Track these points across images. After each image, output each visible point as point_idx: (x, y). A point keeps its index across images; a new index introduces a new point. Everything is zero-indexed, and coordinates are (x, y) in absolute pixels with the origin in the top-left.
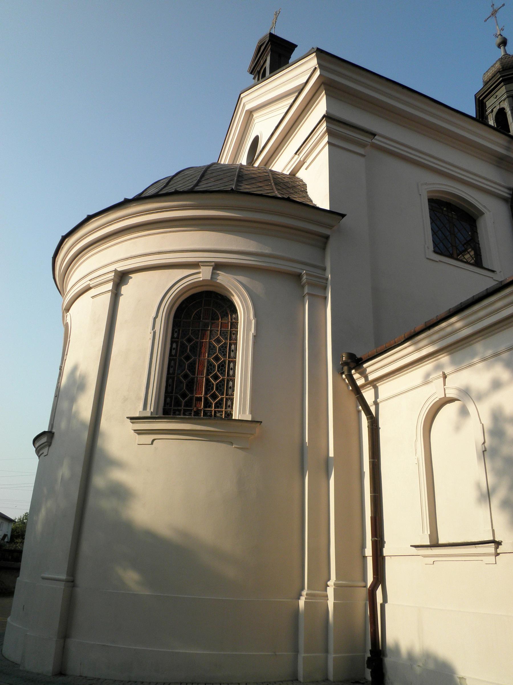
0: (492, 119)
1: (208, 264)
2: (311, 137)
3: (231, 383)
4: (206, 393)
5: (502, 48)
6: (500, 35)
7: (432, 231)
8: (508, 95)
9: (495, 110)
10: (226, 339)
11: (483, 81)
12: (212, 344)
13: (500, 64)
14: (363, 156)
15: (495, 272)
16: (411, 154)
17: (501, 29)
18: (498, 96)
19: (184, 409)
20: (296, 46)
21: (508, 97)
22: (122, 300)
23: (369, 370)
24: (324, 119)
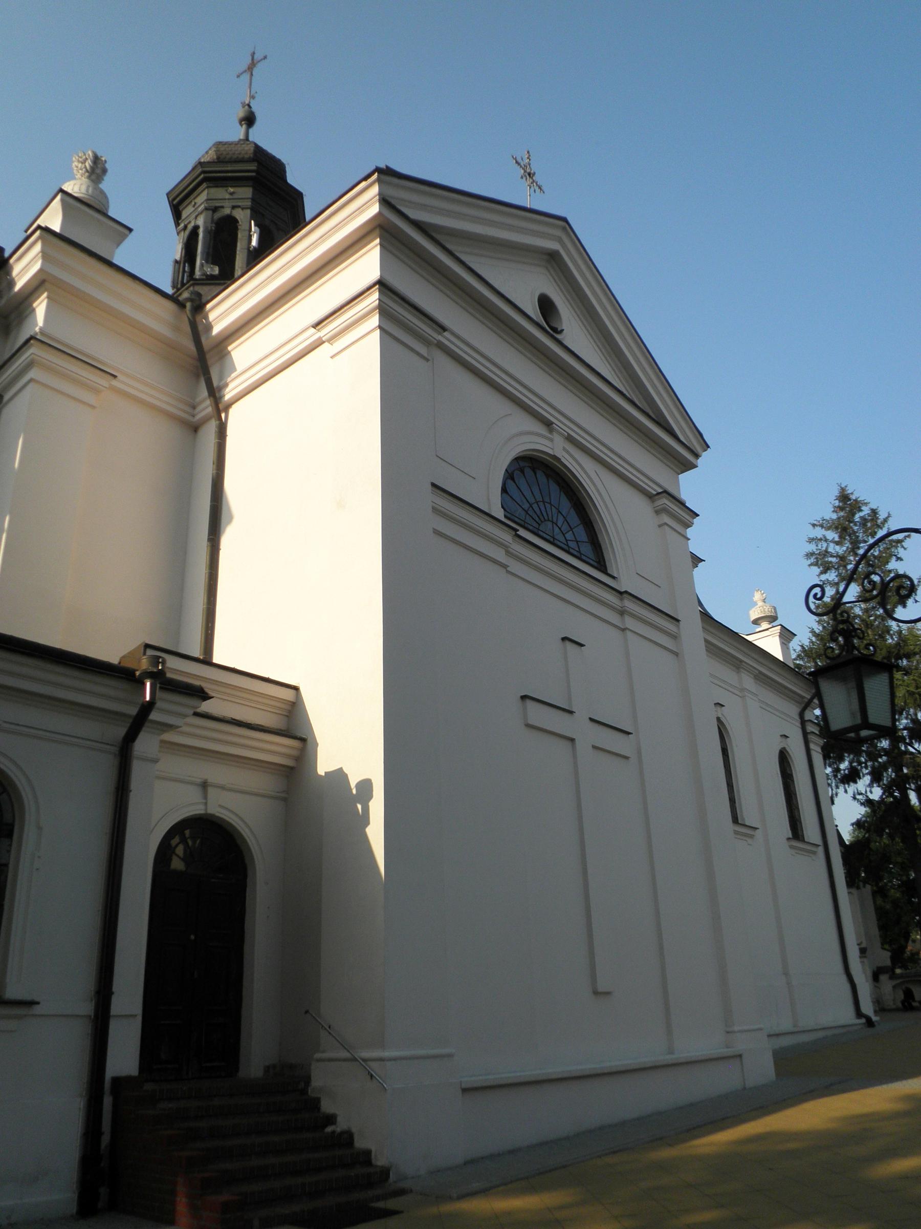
5: (244, 126)
6: (249, 105)
15: (574, 714)
21: (206, 209)
24: (377, 286)
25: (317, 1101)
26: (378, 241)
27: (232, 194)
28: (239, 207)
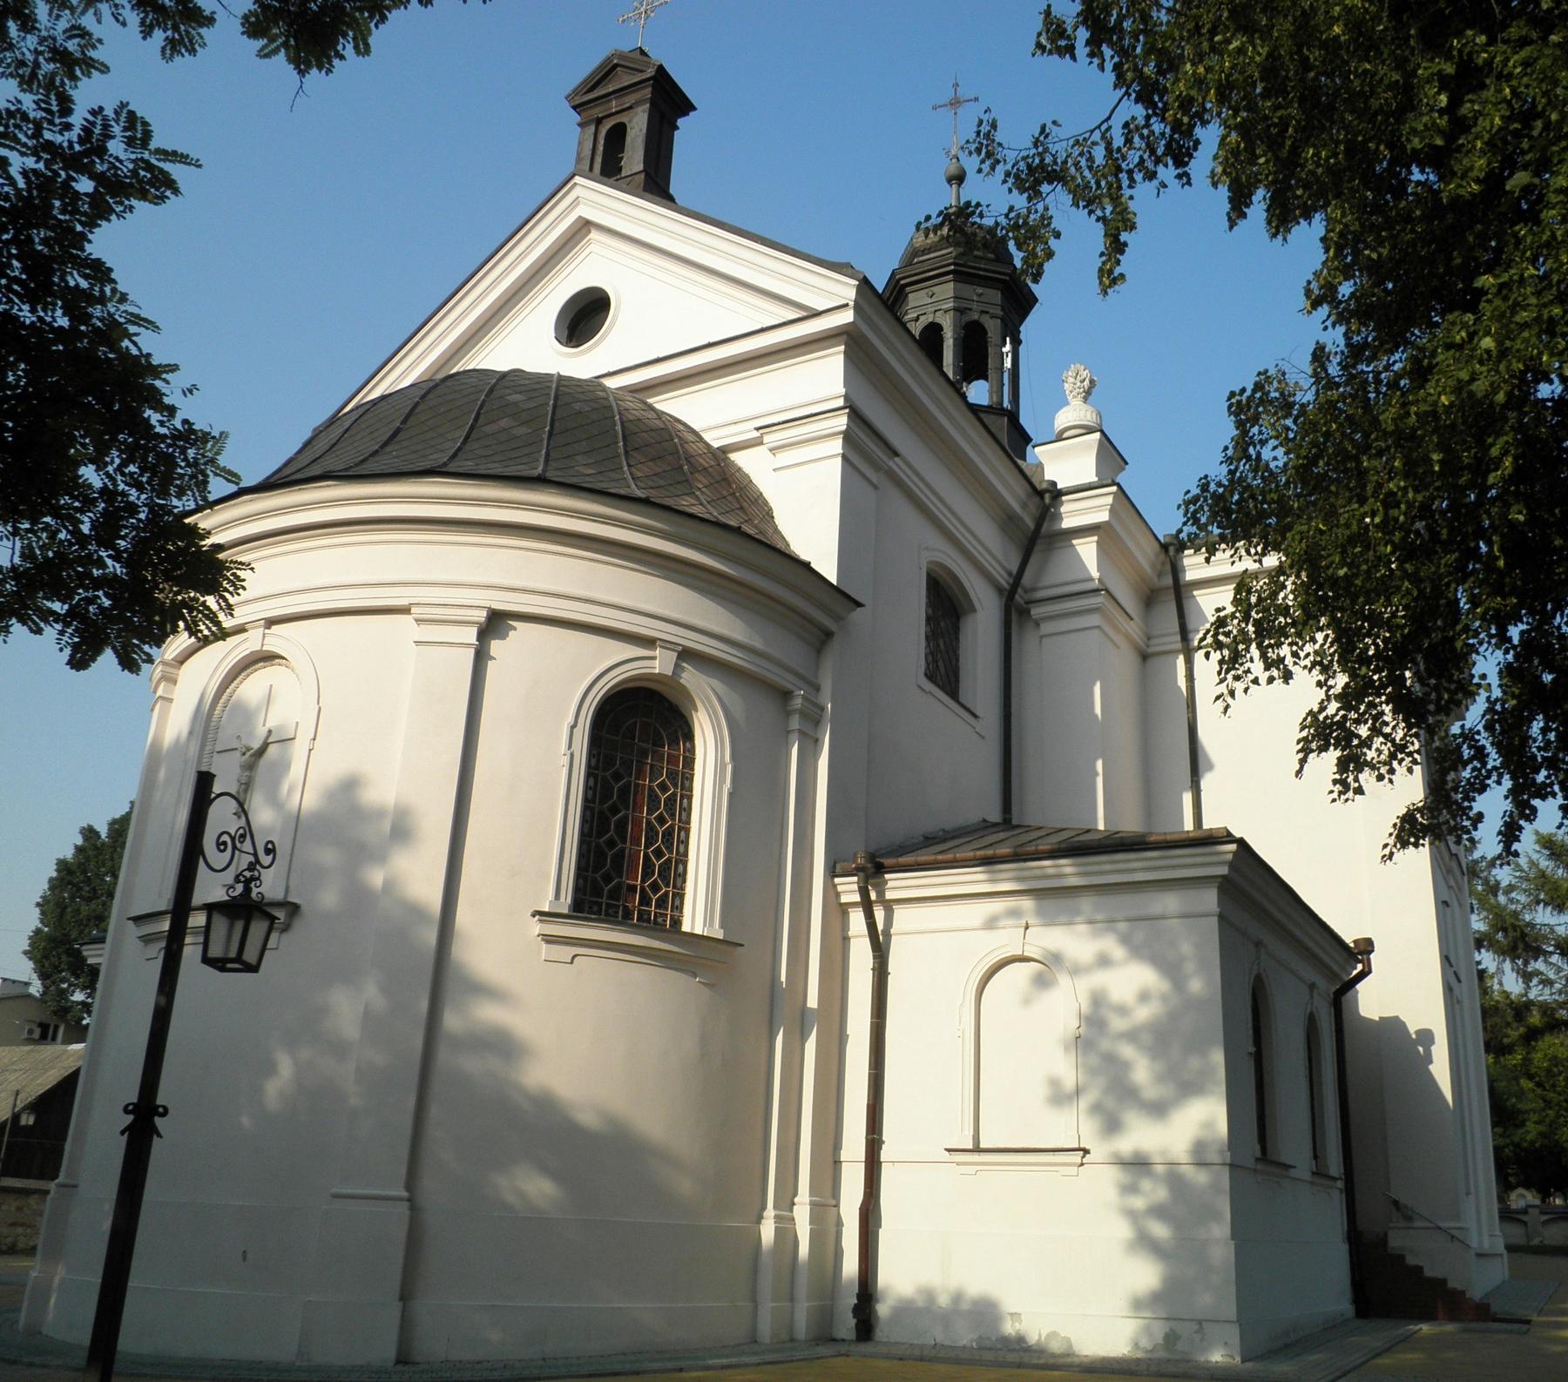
1: (672, 646)
2: (804, 421)
3: (681, 867)
4: (643, 881)
9: (924, 321)
10: (675, 786)
12: (654, 791)
14: (876, 487)
16: (922, 491)
19: (607, 904)
20: (694, 108)
21: (955, 309)
22: (491, 667)
23: (890, 884)
24: (847, 411)
25: (1402, 1257)
26: (842, 348)
28: (987, 312)
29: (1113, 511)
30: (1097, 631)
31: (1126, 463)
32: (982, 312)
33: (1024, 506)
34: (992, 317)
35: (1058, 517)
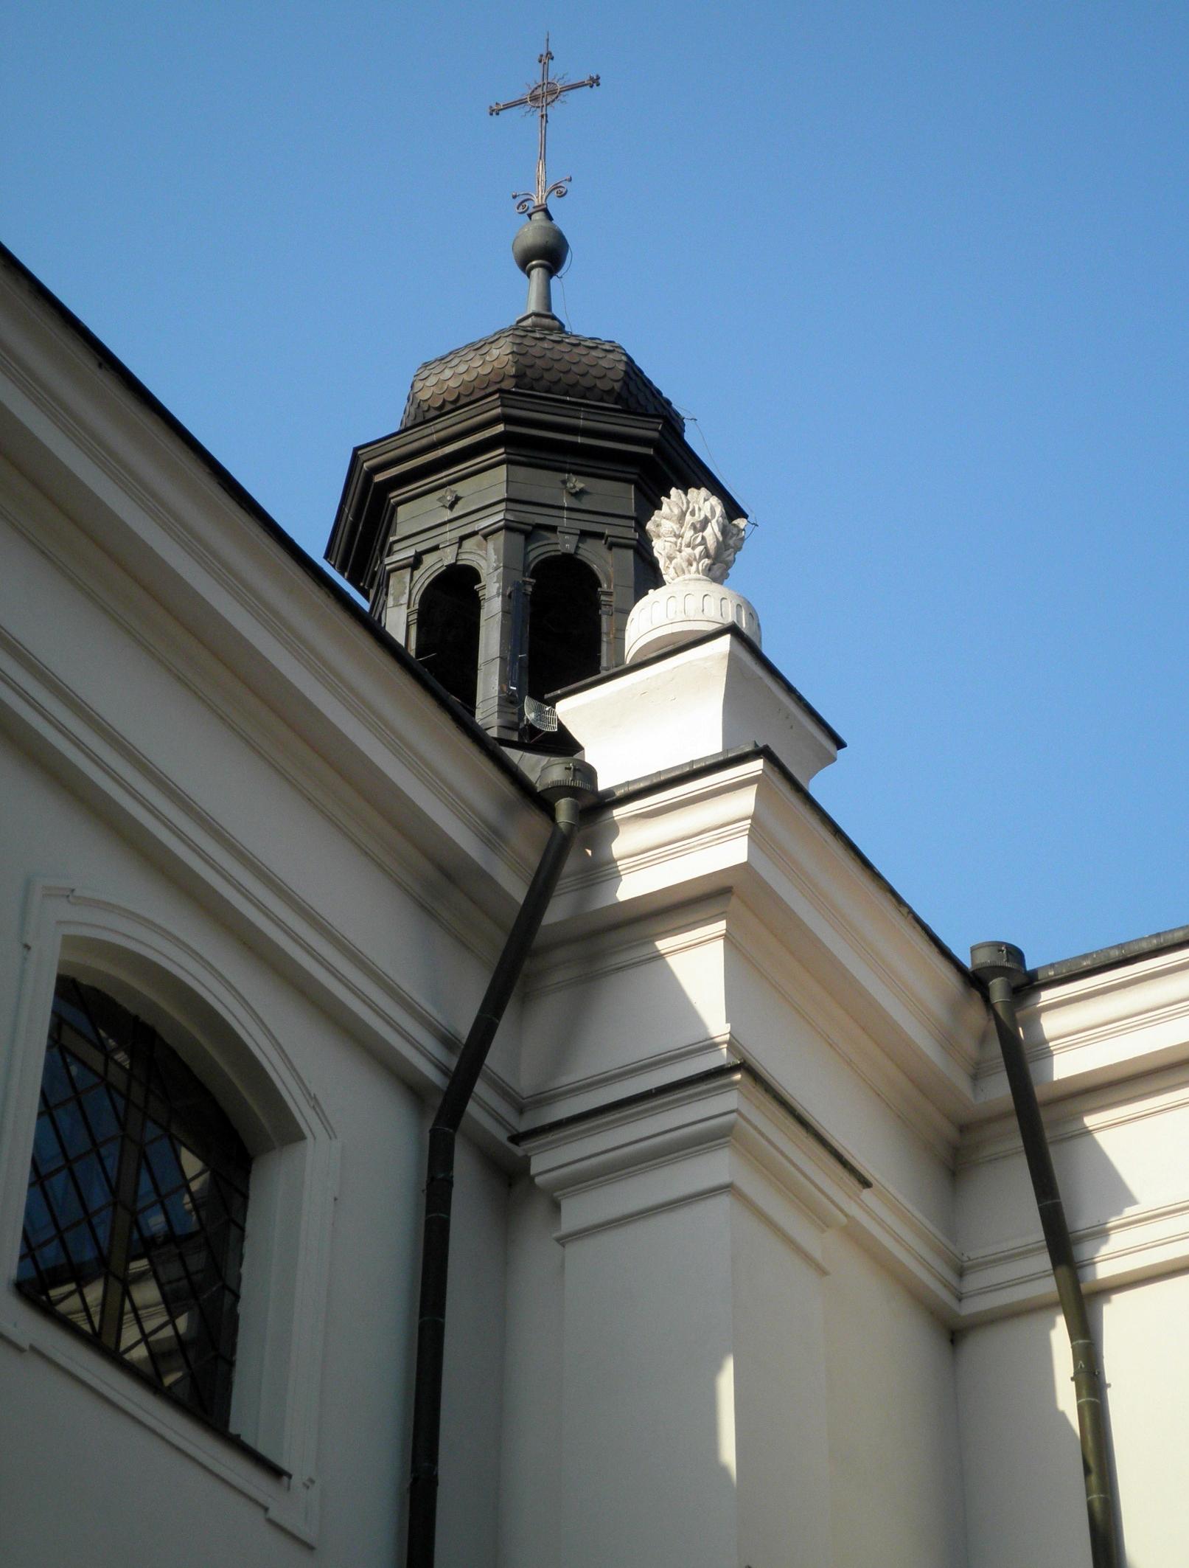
0: (404, 599)
5: (537, 274)
7: (31, 1173)
8: (510, 517)
9: (433, 565)
11: (411, 398)
13: (512, 353)
17: (556, 187)
18: (460, 503)
21: (508, 527)
27: (578, 494)
28: (599, 536)
29: (759, 832)
30: (724, 1201)
31: (840, 744)
32: (584, 535)
33: (492, 837)
34: (611, 546)
35: (603, 872)
